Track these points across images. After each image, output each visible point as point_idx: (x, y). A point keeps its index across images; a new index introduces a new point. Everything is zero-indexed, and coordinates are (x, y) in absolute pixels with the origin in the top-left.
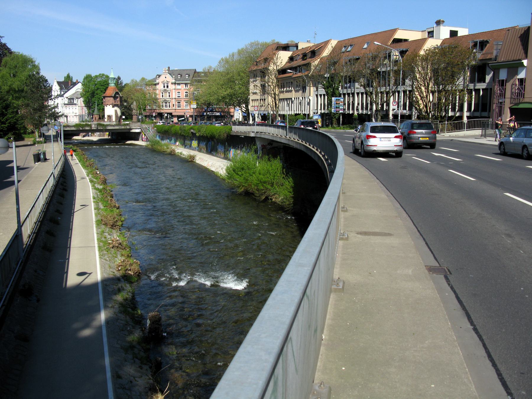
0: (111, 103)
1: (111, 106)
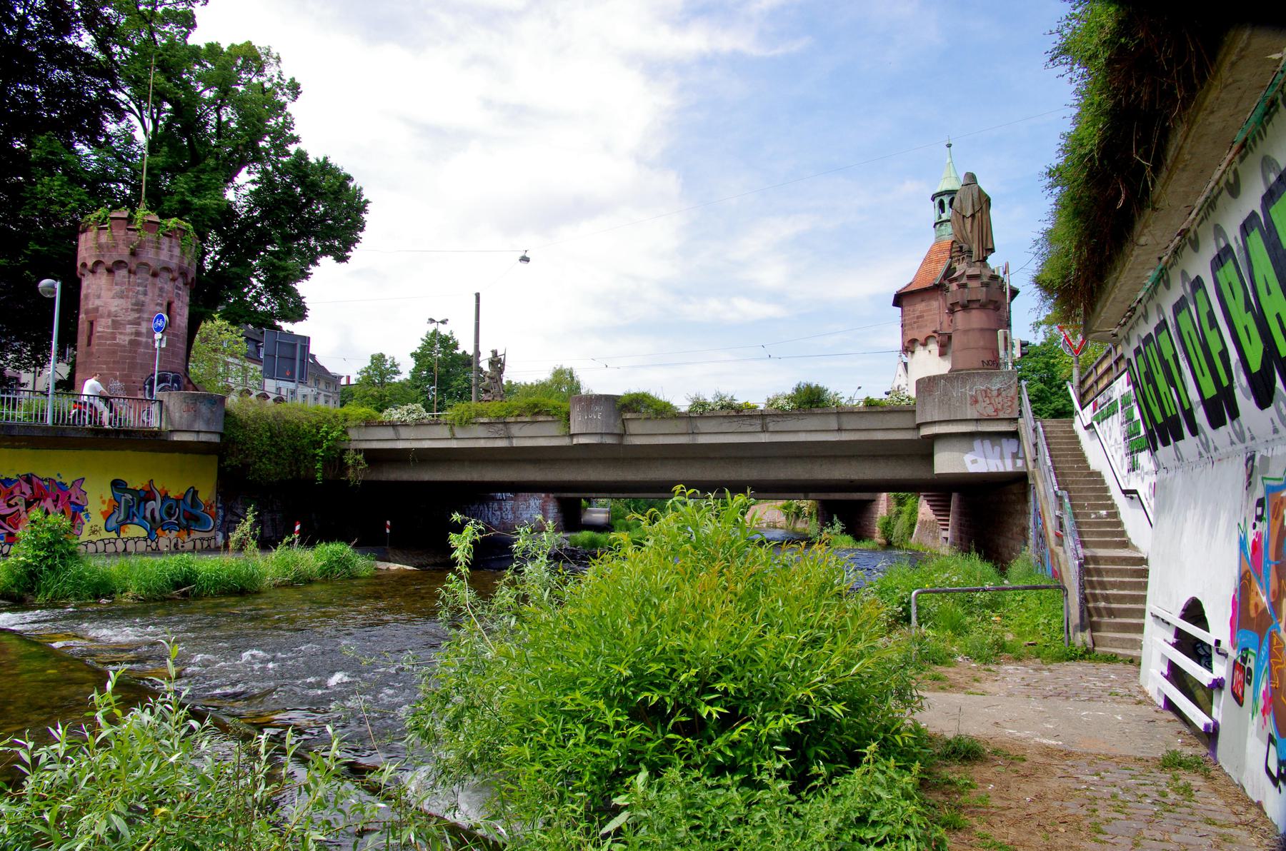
0: (928, 332)
1: (934, 347)
